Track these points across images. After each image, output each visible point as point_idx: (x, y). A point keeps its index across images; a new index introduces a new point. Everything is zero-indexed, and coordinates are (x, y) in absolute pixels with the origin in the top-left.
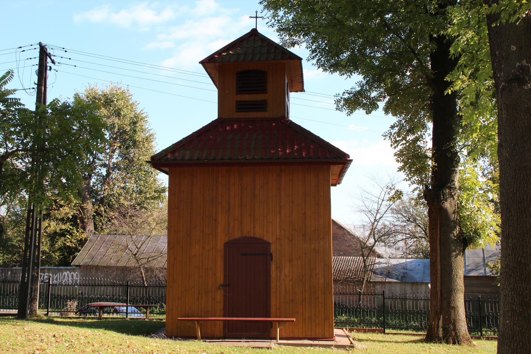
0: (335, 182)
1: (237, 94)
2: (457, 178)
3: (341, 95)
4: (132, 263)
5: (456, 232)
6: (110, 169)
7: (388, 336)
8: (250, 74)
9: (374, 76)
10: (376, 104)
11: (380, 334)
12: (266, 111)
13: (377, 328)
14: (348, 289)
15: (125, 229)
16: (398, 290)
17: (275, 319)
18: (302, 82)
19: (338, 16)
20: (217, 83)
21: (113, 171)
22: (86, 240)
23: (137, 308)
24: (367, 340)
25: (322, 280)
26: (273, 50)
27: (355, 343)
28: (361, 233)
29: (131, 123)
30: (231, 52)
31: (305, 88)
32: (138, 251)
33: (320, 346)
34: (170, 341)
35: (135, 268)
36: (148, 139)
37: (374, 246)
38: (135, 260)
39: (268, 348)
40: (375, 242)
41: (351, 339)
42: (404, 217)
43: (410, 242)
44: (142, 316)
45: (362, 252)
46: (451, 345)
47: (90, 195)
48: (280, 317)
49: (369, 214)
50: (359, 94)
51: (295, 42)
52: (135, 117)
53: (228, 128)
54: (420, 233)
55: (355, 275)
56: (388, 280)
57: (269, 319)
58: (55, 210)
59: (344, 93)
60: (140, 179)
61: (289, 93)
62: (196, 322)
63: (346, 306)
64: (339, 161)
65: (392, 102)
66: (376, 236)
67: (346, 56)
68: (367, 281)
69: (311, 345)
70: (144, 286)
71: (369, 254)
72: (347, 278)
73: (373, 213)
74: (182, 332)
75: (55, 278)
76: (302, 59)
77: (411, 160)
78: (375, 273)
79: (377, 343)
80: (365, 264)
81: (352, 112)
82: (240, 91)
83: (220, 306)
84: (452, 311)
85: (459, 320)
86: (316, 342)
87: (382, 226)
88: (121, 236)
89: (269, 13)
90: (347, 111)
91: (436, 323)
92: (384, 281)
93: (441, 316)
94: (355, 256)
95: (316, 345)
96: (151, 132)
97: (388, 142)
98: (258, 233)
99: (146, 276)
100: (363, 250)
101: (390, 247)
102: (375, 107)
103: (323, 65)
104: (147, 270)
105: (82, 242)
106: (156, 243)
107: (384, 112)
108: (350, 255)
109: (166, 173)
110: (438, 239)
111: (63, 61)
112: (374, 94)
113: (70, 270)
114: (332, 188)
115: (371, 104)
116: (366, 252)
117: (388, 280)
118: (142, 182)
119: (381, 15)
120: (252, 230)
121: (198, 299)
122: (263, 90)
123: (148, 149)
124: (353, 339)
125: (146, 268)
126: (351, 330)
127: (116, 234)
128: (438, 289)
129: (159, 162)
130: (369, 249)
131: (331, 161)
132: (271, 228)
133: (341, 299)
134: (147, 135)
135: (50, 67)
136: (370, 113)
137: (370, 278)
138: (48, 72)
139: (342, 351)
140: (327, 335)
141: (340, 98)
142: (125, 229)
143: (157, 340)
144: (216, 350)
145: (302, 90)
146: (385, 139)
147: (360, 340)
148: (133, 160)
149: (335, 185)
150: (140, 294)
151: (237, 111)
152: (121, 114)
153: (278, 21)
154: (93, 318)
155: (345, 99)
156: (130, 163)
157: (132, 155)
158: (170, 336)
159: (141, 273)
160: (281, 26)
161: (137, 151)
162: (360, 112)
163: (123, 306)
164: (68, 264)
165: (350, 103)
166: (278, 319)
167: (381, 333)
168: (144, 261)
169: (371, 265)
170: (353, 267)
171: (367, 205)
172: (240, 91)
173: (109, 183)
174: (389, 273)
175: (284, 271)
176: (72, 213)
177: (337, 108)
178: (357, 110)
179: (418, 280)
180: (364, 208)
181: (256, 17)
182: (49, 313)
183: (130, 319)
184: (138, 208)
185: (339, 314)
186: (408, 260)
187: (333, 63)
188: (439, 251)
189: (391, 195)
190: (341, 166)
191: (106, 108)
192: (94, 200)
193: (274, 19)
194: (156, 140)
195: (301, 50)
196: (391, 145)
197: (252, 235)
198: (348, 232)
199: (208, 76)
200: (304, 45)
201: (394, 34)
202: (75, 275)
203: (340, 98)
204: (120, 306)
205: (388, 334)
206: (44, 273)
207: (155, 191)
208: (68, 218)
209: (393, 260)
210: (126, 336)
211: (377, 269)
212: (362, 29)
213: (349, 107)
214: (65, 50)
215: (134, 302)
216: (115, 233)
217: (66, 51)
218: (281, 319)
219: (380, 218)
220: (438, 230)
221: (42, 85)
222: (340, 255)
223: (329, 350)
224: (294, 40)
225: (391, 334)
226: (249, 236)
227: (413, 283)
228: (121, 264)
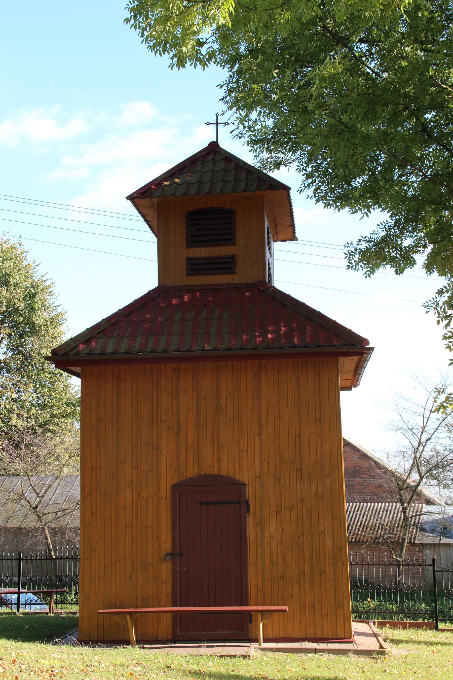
0: (348, 383)
1: (188, 246)
3: (355, 245)
4: (31, 522)
7: (444, 634)
8: (207, 214)
9: (408, 212)
10: (412, 258)
11: (429, 631)
13: (426, 621)
14: (375, 556)
15: (20, 466)
17: (256, 608)
18: (292, 225)
19: (345, 118)
23: (35, 595)
24: (407, 642)
25: (329, 544)
26: (244, 176)
27: (387, 646)
28: (398, 465)
29: (26, 296)
30: (177, 180)
31: (298, 234)
32: (40, 502)
33: (330, 651)
34: (85, 650)
35: (35, 529)
36: (54, 322)
37: (418, 485)
38: (35, 517)
39: (244, 657)
40: (421, 478)
41: (381, 639)
44: (45, 608)
45: (400, 495)
48: (263, 605)
49: (409, 434)
51: (281, 161)
52: (33, 286)
55: (389, 533)
56: (444, 540)
57: (246, 608)
60: (43, 387)
61: (272, 243)
62: (128, 616)
63: (373, 585)
64: (351, 351)
65: (438, 254)
66: (423, 470)
67: (360, 181)
68: (409, 542)
69: (315, 651)
70: (51, 558)
71: (411, 499)
72: (376, 538)
73: (416, 432)
74: (107, 636)
76: (290, 189)
78: (422, 529)
79: (424, 646)
80: (405, 516)
81: (372, 272)
82: (192, 241)
83: (166, 589)
87: (432, 453)
88: (12, 478)
89: (232, 115)
90: (366, 270)
92: (437, 542)
94: (389, 502)
96: (59, 310)
97: (433, 316)
99: (53, 542)
100: (402, 492)
101: (446, 486)
103: (324, 198)
104: (54, 532)
106: (69, 489)
107: (424, 271)
108: (380, 500)
109: (77, 375)
114: (343, 394)
115: (402, 257)
116: (406, 496)
117: (444, 540)
118: (46, 390)
119: (417, 113)
120: (216, 464)
121: (131, 577)
122: (229, 239)
123: (55, 338)
124: (385, 640)
125: (53, 529)
126: (381, 625)
127: (3, 475)
129: (67, 357)
130: (411, 490)
131: (337, 351)
132: (243, 460)
133: (361, 572)
134: (52, 314)
136: (402, 272)
137: (415, 538)
139: (365, 661)
141: (353, 250)
142: (20, 466)
143: (65, 648)
144: (159, 662)
146: (427, 312)
147: (394, 641)
148: (30, 357)
149: (349, 388)
150: (39, 573)
151: (188, 275)
152: (9, 282)
153: (249, 127)
155: (361, 251)
156: (26, 359)
157: (28, 348)
158: (88, 641)
159: (46, 539)
160: (254, 135)
161: (35, 340)
162: (386, 272)
163: (12, 593)
165: (370, 257)
166: (260, 608)
167: (431, 629)
169: (416, 515)
170: (387, 519)
172: (192, 241)
174: (445, 528)
177: (349, 266)
178: (381, 269)
180: (401, 425)
181: (217, 124)
183: (23, 614)
184: (40, 431)
185: (361, 597)
187: (341, 194)
189: (438, 403)
190: (355, 358)
193: (243, 124)
194: (67, 323)
195: (289, 175)
196: (438, 323)
197: (216, 472)
198: (376, 463)
199: (142, 219)
200: (295, 165)
201: (438, 144)
203: (353, 250)
204: (7, 593)
205: (443, 630)
207: (68, 404)
210: (14, 643)
211: (426, 523)
212: (384, 138)
213: (368, 264)
215: (32, 585)
218: (265, 608)
219: (427, 440)
222: (364, 501)
223: (343, 658)
224: (278, 158)
225: (449, 630)
226: (212, 473)
228: (14, 523)
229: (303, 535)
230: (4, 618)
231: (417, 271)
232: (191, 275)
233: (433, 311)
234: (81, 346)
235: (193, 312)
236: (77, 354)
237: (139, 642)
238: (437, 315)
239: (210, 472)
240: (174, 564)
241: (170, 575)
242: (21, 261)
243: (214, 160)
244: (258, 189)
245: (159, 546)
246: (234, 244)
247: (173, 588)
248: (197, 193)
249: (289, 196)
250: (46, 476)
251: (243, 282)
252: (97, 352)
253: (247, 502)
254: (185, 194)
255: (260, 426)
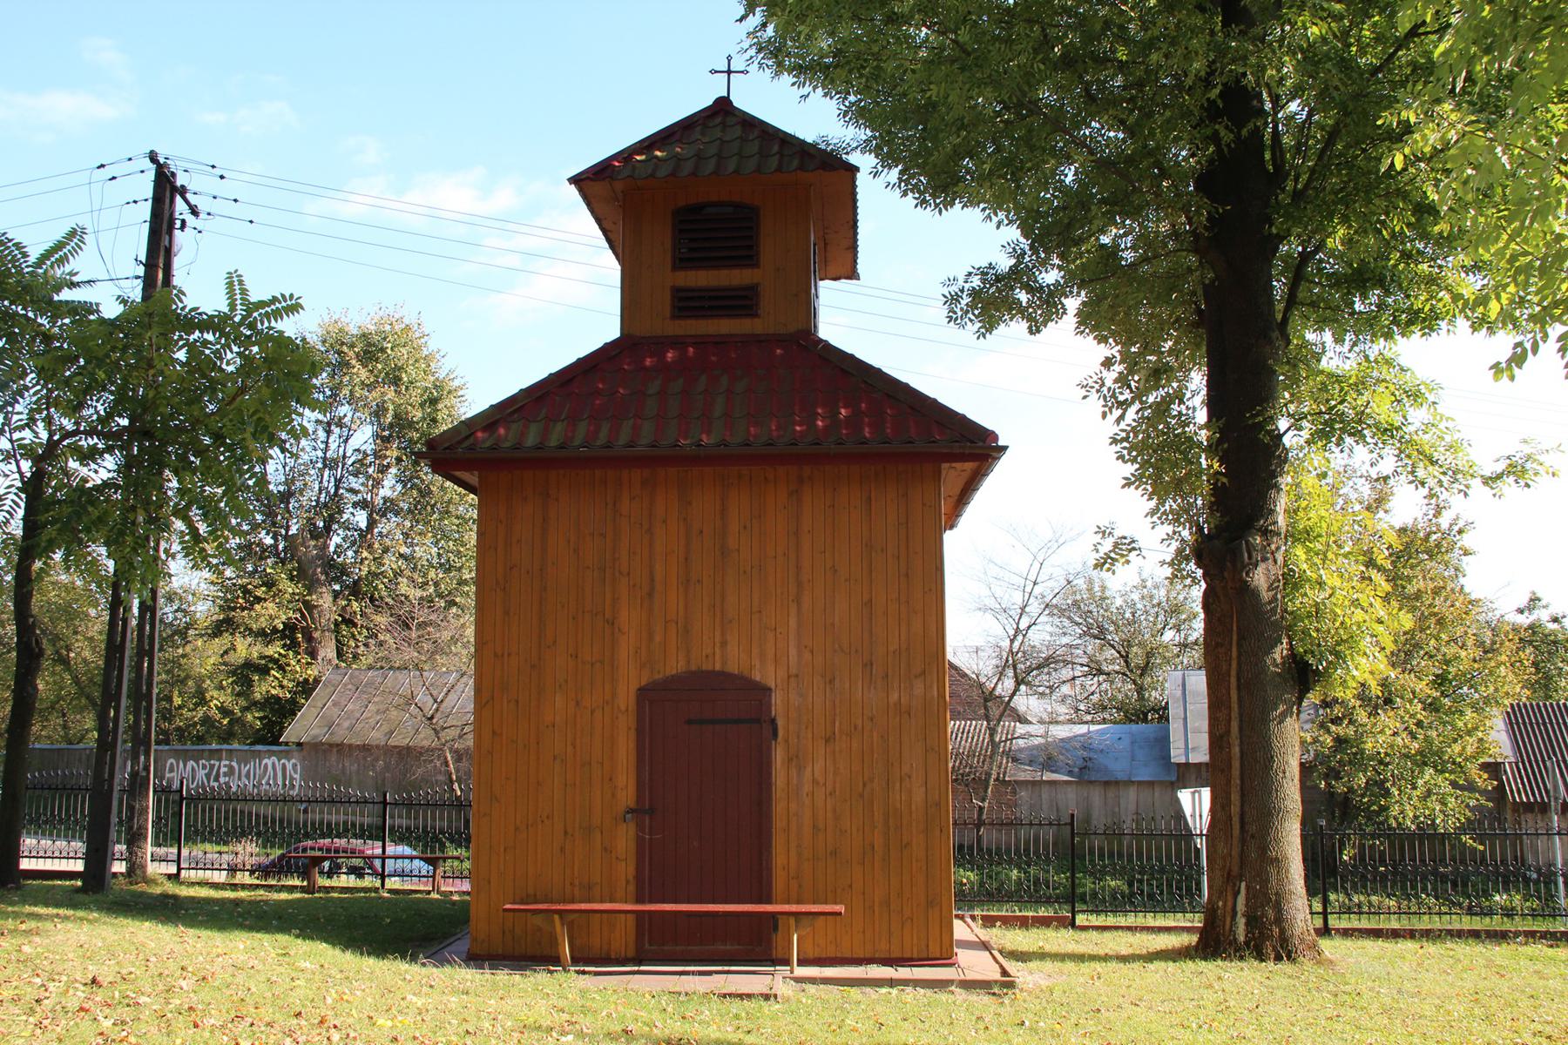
1: (675, 268)
2: (1282, 503)
3: (961, 283)
4: (425, 738)
5: (1280, 652)
6: (377, 513)
7: (1083, 935)
8: (709, 218)
11: (1063, 931)
12: (756, 315)
15: (410, 654)
16: (1070, 801)
20: (620, 251)
21: (384, 515)
22: (317, 681)
25: (918, 796)
26: (776, 148)
30: (658, 153)
31: (861, 268)
35: (430, 750)
39: (767, 997)
42: (1078, 624)
43: (1092, 683)
46: (1271, 965)
47: (327, 575)
48: (798, 902)
49: (1002, 617)
50: (1018, 275)
53: (648, 362)
54: (1113, 662)
56: (1048, 776)
58: (243, 609)
59: (970, 274)
62: (556, 917)
68: (997, 779)
69: (892, 983)
71: (1001, 715)
74: (518, 949)
75: (244, 772)
77: (1156, 457)
78: (1015, 760)
82: (682, 262)
83: (626, 870)
84: (1273, 871)
85: (1291, 893)
86: (904, 972)
91: (1230, 904)
93: (1243, 885)
95: (905, 982)
97: (1095, 404)
98: (733, 659)
99: (457, 771)
102: (1057, 312)
105: (307, 687)
110: (1233, 673)
111: (214, 207)
112: (1050, 277)
113: (280, 755)
117: (1048, 776)
121: (562, 850)
122: (748, 257)
125: (457, 751)
128: (1235, 809)
131: (948, 453)
135: (183, 222)
136: (1038, 331)
138: (177, 233)
139: (980, 1000)
140: (934, 950)
142: (410, 654)
145: (852, 274)
148: (431, 492)
151: (674, 317)
154: (292, 889)
164: (275, 742)
166: (794, 908)
168: (453, 733)
171: (999, 592)
172: (682, 262)
173: (370, 546)
175: (809, 769)
176: (284, 618)
179: (1121, 776)
180: (992, 603)
181: (729, 72)
182: (183, 872)
183: (390, 891)
186: (1093, 728)
188: (1235, 706)
190: (969, 466)
191: (365, 366)
192: (337, 587)
196: (1104, 415)
197: (718, 667)
202: (289, 766)
205: (1084, 928)
206: (220, 760)
208: (275, 630)
209: (1059, 727)
211: (1021, 750)
214: (218, 172)
216: (385, 665)
217: (222, 177)
220: (1234, 649)
221: (157, 266)
223: (943, 997)
227: (1107, 783)
229: (872, 780)
230: (356, 899)
231: (1063, 331)
232: (679, 317)
233: (1094, 395)
234: (480, 434)
235: (681, 381)
236: (471, 448)
237: (576, 961)
238: (1102, 402)
239: (707, 667)
240: (640, 827)
241: (632, 845)
242: (418, 349)
243: (723, 123)
244: (801, 168)
245: (613, 795)
246: (756, 265)
247: (637, 869)
248: (694, 174)
249: (854, 187)
250: (449, 672)
251: (771, 331)
252: (508, 444)
253: (773, 721)
254: (673, 174)
255: (799, 585)
